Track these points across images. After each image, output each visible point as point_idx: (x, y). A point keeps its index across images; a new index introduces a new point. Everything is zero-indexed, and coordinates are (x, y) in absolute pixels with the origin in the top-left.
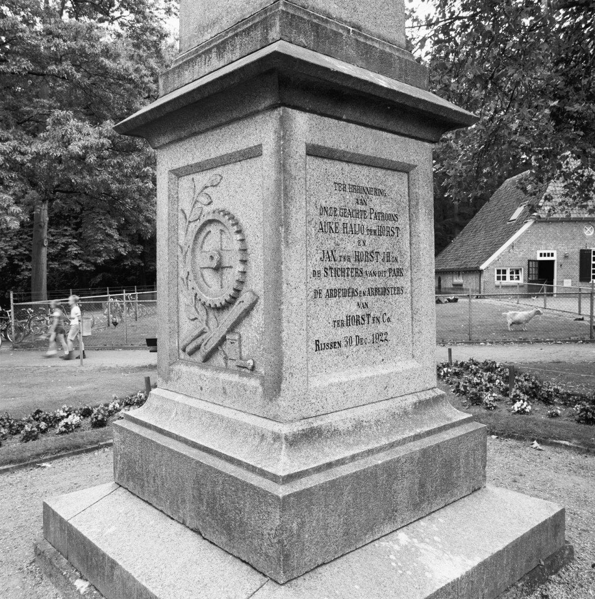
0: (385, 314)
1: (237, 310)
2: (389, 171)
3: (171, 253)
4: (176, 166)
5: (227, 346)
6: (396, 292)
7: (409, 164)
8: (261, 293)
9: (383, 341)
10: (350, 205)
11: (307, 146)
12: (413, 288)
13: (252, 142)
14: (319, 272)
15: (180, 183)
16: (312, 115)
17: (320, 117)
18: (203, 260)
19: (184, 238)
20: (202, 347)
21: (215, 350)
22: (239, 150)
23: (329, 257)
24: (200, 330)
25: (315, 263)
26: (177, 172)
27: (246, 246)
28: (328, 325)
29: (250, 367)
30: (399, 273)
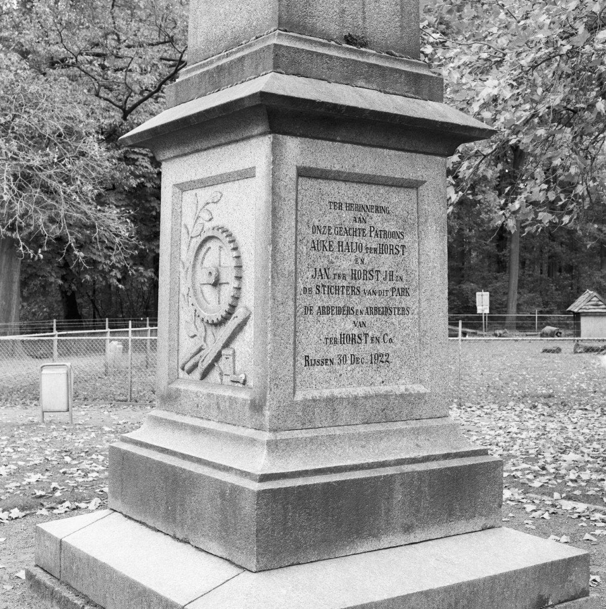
1: (232, 324)
2: (393, 188)
3: (173, 270)
4: (180, 181)
5: (222, 362)
6: (400, 312)
8: (252, 309)
9: (383, 362)
10: (347, 223)
11: (298, 169)
12: (421, 309)
14: (310, 289)
16: (304, 139)
17: (312, 140)
18: (202, 276)
19: (186, 255)
20: (200, 364)
21: (211, 367)
23: (322, 275)
24: (198, 347)
25: (306, 280)
26: (181, 187)
27: (241, 263)
28: (320, 342)
29: (242, 381)
30: (404, 292)
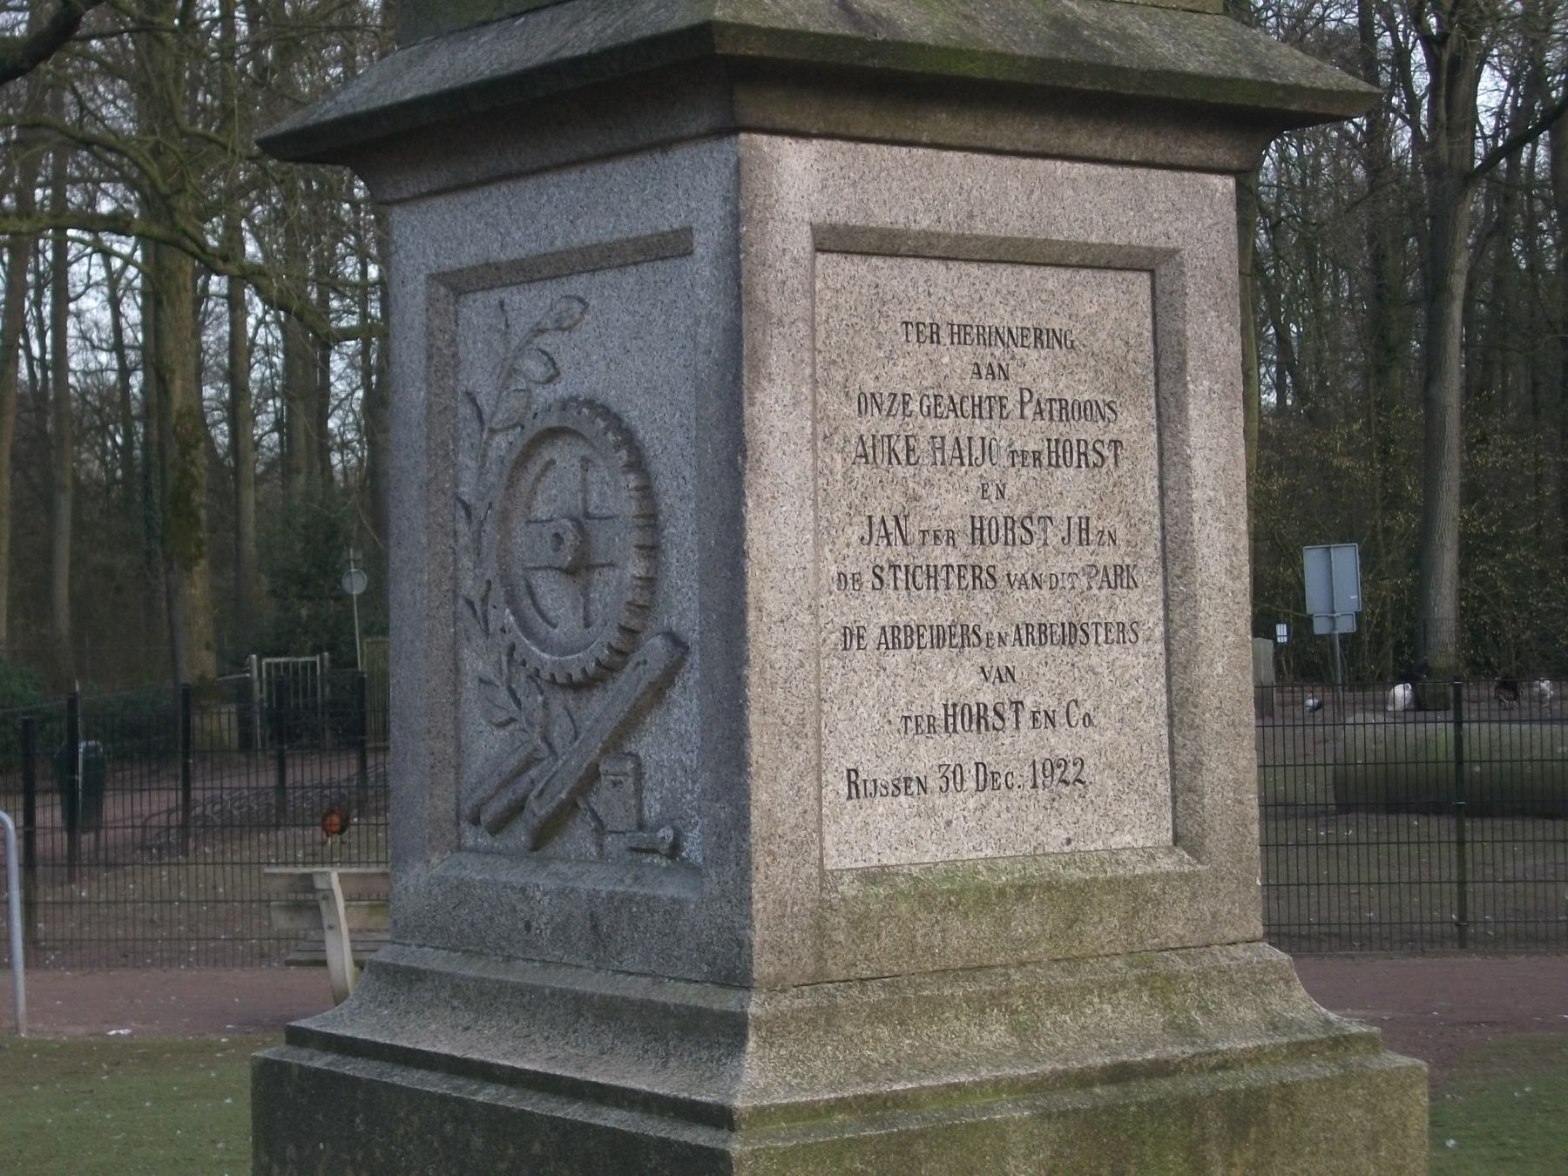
0: (1076, 702)
1: (630, 684)
2: (1084, 272)
4: (449, 264)
5: (603, 798)
7: (1150, 249)
9: (1066, 783)
10: (955, 381)
11: (816, 230)
13: (668, 219)
15: (465, 312)
22: (631, 236)
23: (887, 535)
25: (845, 551)
28: (887, 727)
29: (665, 847)
